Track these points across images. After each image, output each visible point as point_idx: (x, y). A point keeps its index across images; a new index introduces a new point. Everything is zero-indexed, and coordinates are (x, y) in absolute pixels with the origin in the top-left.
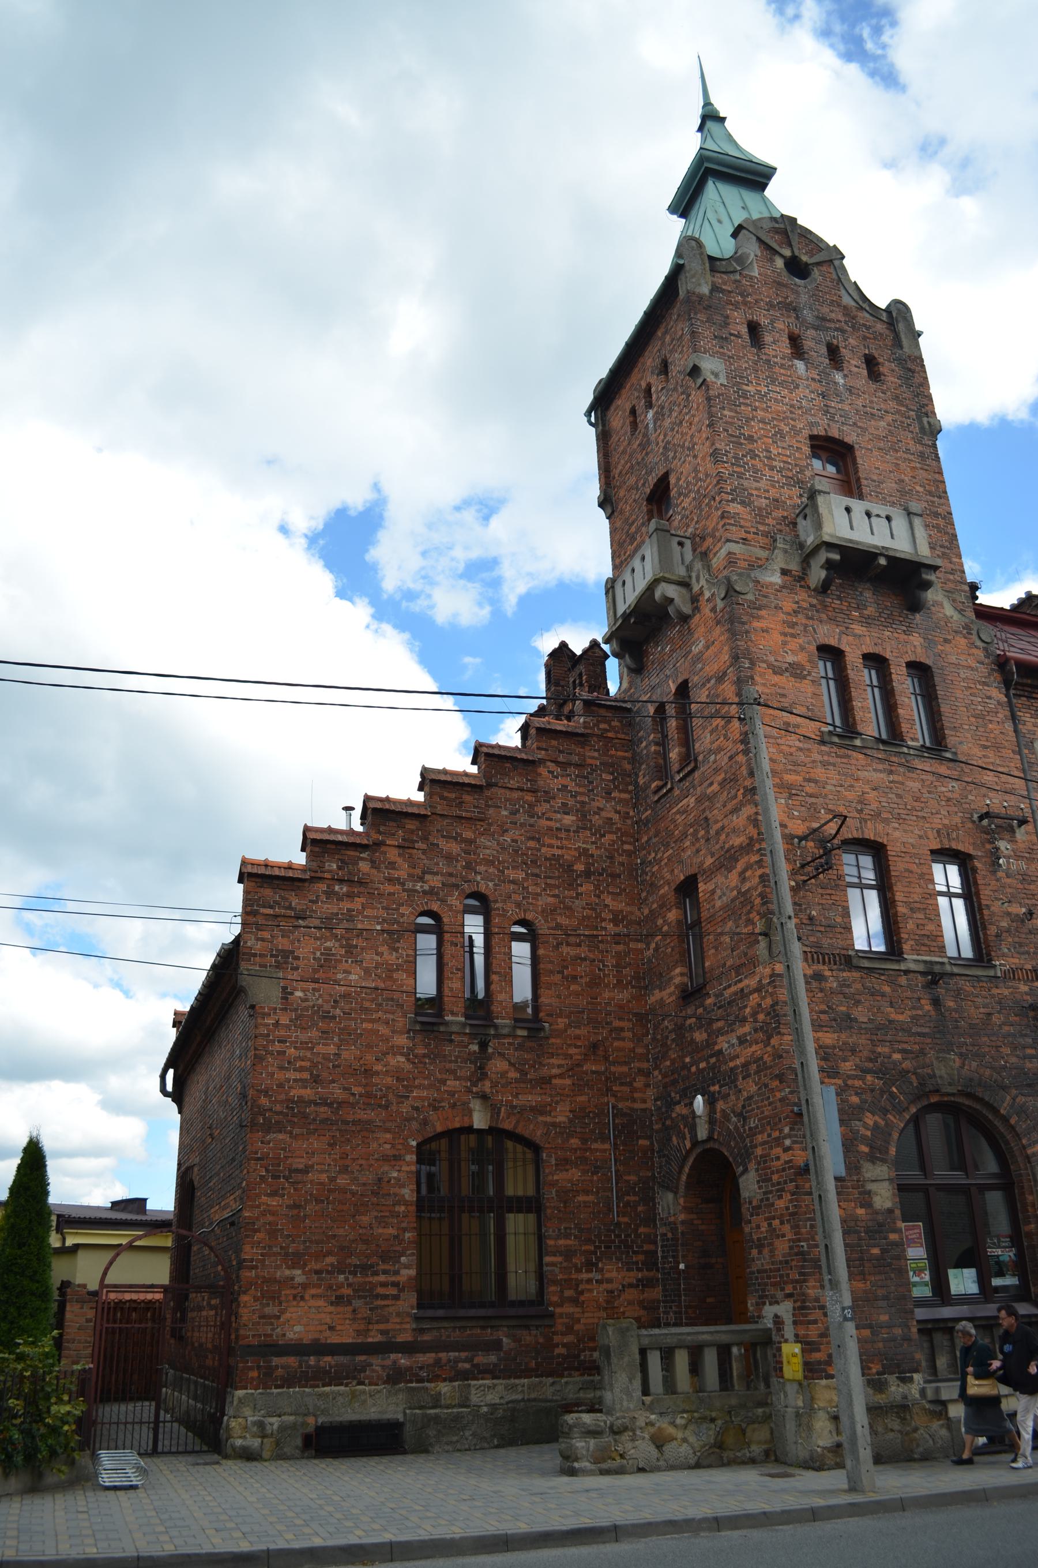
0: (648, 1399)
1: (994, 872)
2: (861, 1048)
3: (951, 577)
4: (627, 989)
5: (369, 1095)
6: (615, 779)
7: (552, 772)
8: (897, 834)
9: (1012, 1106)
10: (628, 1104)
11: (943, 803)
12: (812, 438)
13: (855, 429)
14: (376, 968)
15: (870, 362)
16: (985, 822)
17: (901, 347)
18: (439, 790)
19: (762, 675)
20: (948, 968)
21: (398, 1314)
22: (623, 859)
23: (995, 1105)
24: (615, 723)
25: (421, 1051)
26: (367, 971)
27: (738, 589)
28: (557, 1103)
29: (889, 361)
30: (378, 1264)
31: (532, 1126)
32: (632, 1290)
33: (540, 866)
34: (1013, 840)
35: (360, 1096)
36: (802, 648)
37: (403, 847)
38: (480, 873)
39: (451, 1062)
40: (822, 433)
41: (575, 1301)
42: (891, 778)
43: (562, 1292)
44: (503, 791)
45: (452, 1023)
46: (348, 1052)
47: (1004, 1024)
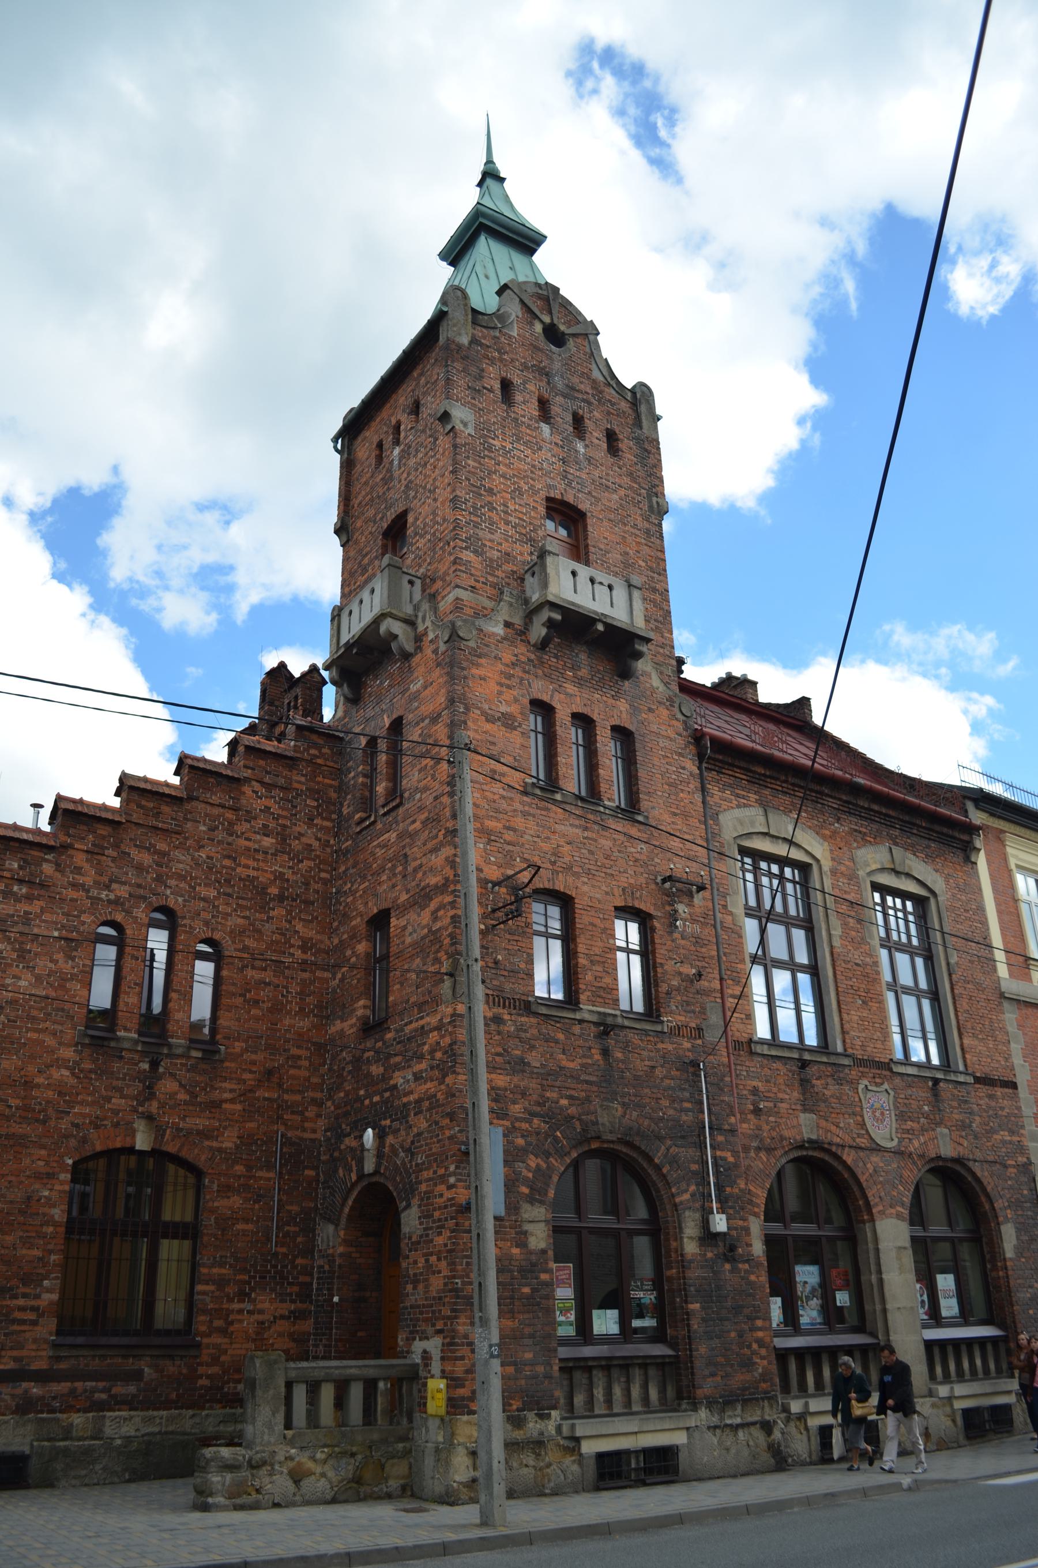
0: (289, 1433)
1: (671, 933)
2: (531, 1091)
3: (661, 651)
4: (308, 1017)
5: (26, 1108)
6: (319, 806)
7: (256, 792)
8: (585, 888)
9: (665, 1156)
10: (298, 1133)
11: (631, 863)
12: (548, 499)
13: (589, 498)
14: (49, 975)
15: (611, 437)
16: (667, 885)
17: (641, 428)
18: (136, 798)
19: (475, 721)
20: (620, 1020)
21: (35, 1341)
22: (318, 886)
23: (651, 1154)
24: (325, 750)
25: (87, 1065)
26: (38, 978)
27: (461, 635)
28: (225, 1128)
29: (628, 439)
30: (18, 1287)
31: (196, 1151)
32: (282, 1322)
33: (234, 886)
34: (690, 905)
35: (17, 1108)
36: (516, 700)
37: (92, 853)
38: (170, 887)
39: (118, 1079)
40: (559, 497)
41: (224, 1332)
42: (586, 834)
43: (211, 1322)
44: (203, 805)
45: (124, 1039)
46: (8, 1062)
47: (666, 1077)
